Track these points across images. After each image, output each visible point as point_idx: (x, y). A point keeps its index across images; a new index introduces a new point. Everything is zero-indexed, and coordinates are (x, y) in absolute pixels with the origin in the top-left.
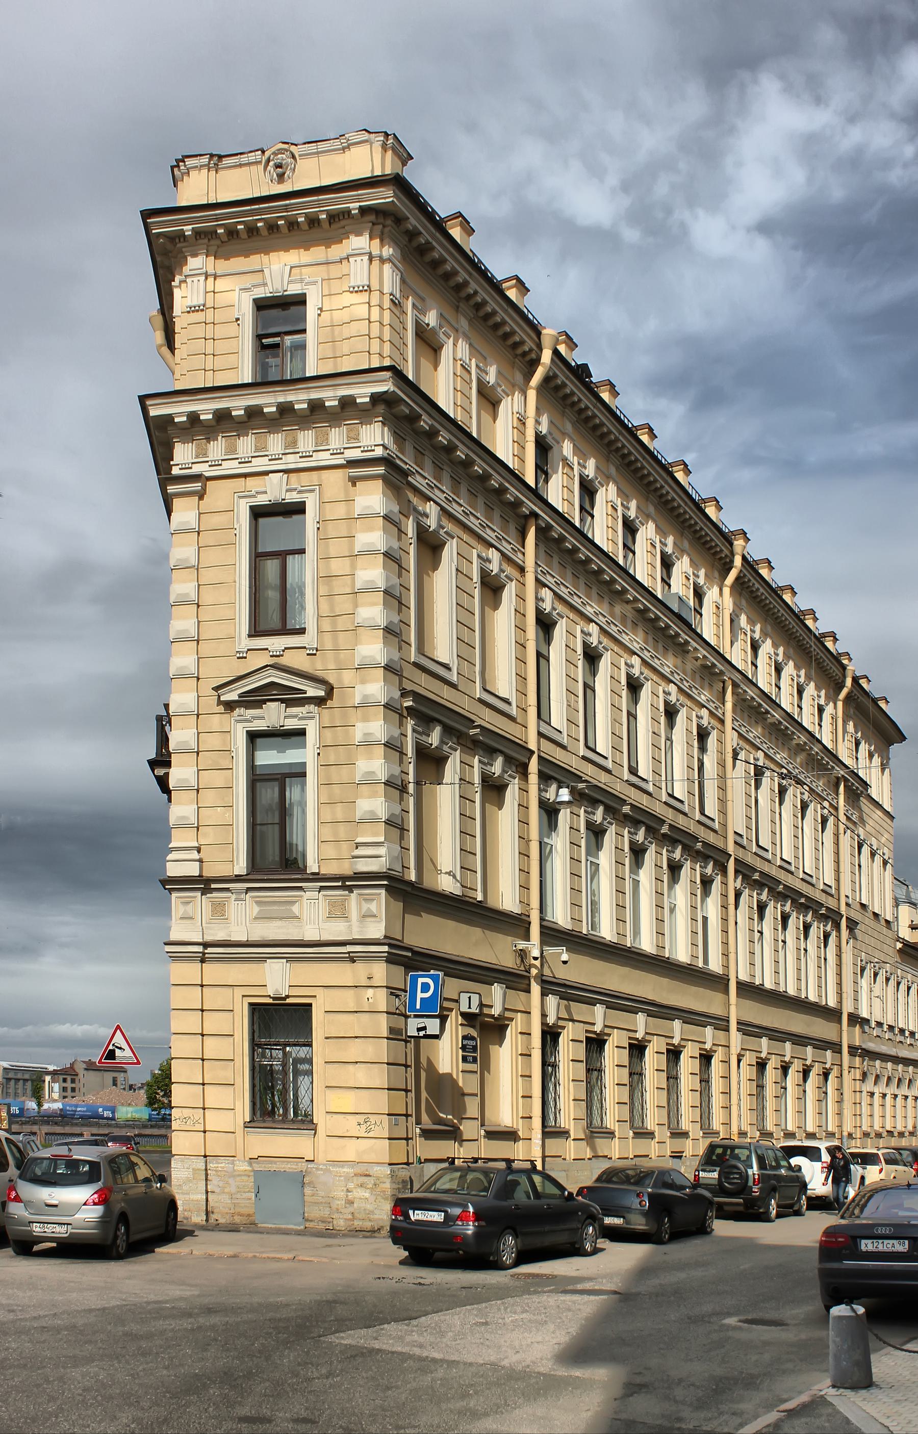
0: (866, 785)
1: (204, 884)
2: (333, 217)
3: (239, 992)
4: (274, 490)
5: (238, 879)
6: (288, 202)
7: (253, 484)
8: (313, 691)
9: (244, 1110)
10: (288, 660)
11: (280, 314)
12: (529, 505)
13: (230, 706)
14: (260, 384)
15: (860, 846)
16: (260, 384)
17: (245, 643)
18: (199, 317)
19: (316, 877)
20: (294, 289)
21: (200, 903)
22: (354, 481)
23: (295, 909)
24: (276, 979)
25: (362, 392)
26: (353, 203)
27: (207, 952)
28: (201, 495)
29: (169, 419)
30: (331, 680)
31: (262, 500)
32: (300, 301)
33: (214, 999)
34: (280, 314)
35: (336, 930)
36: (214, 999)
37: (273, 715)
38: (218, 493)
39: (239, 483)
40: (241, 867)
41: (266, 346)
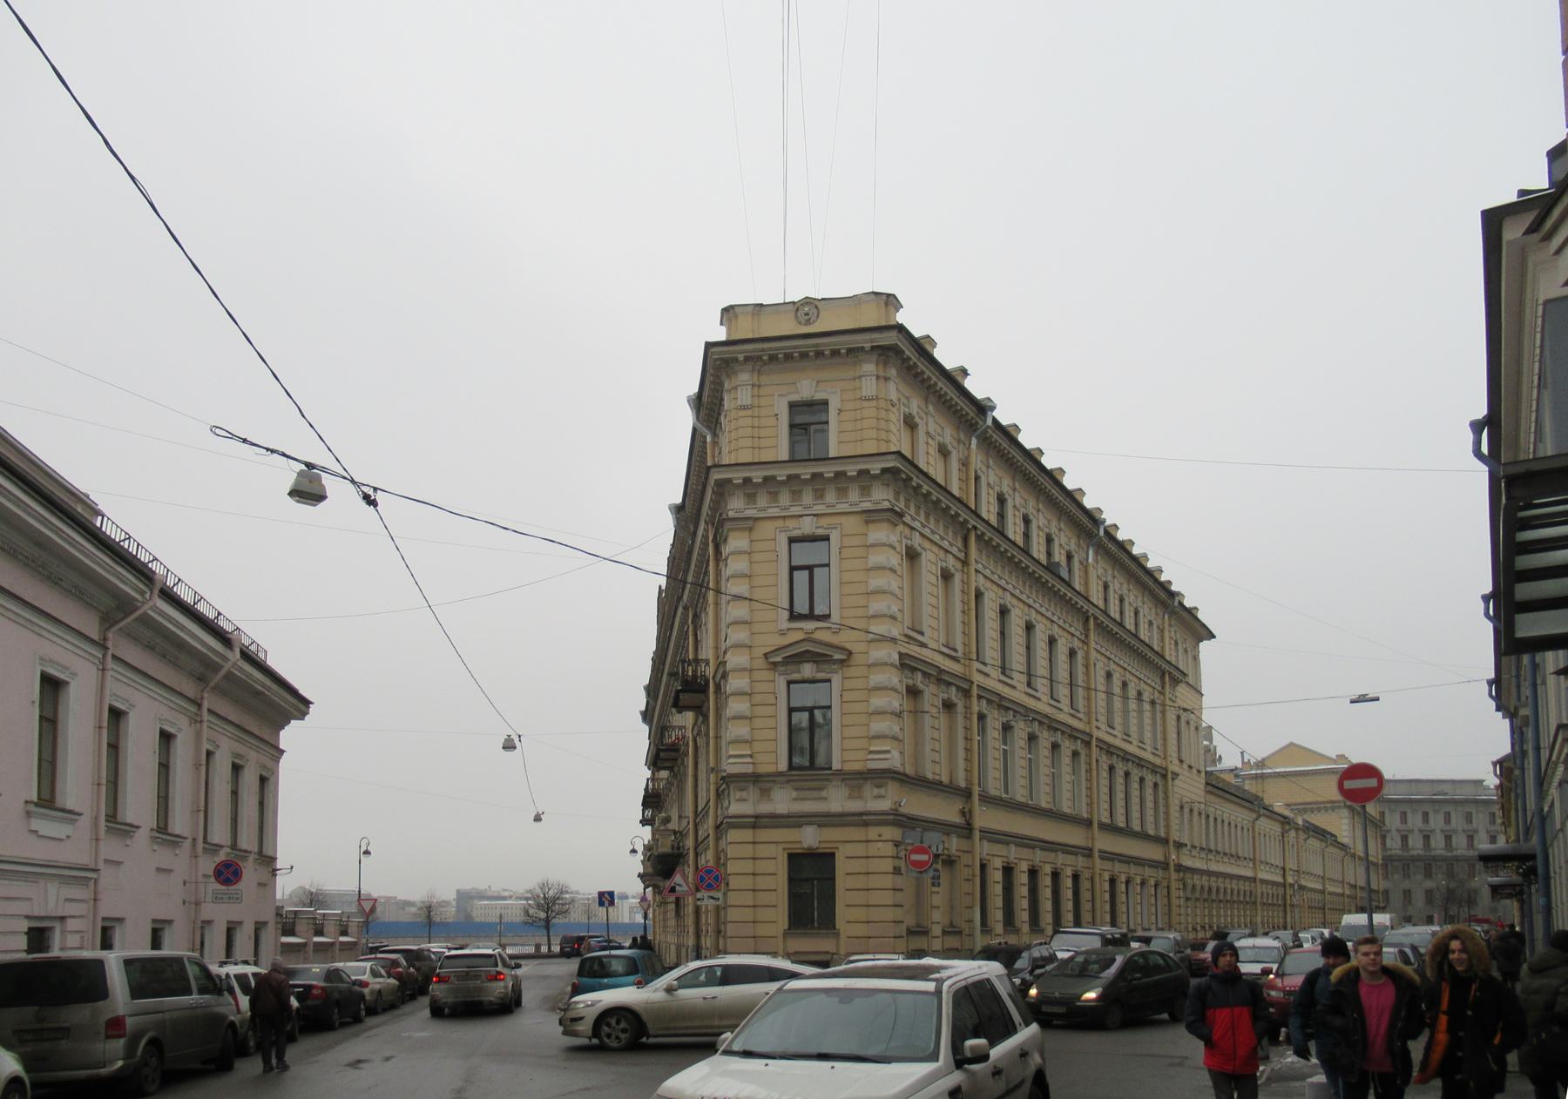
0: (1185, 675)
1: (755, 779)
2: (850, 351)
3: (781, 847)
4: (807, 526)
5: (781, 774)
6: (87, 561)
7: (791, 523)
8: (837, 656)
9: (783, 921)
10: (819, 636)
11: (807, 419)
12: (972, 522)
13: (775, 664)
14: (792, 461)
15: (1087, 619)
16: (792, 461)
17: (785, 625)
18: (749, 413)
19: (839, 773)
20: (819, 396)
21: (752, 793)
22: (867, 522)
23: (824, 793)
24: (809, 838)
25: (875, 467)
26: (864, 341)
27: (757, 822)
28: (751, 529)
29: (729, 481)
30: (848, 646)
31: (796, 533)
32: (825, 403)
33: (764, 851)
34: (807, 419)
35: (855, 806)
36: (764, 851)
37: (808, 670)
38: (766, 529)
39: (780, 523)
40: (783, 766)
41: (799, 429)
